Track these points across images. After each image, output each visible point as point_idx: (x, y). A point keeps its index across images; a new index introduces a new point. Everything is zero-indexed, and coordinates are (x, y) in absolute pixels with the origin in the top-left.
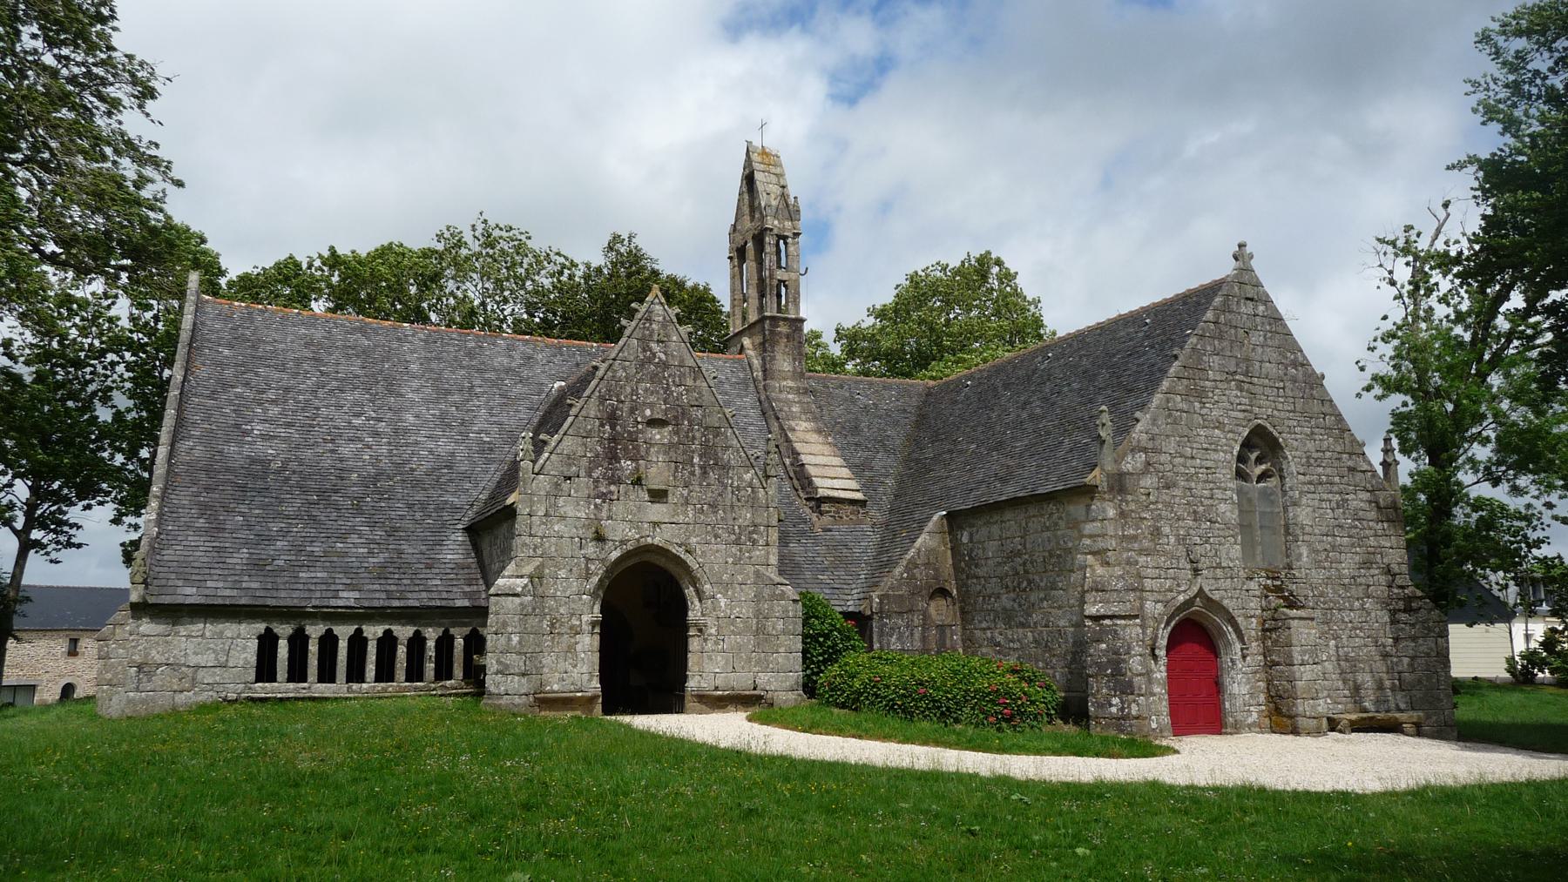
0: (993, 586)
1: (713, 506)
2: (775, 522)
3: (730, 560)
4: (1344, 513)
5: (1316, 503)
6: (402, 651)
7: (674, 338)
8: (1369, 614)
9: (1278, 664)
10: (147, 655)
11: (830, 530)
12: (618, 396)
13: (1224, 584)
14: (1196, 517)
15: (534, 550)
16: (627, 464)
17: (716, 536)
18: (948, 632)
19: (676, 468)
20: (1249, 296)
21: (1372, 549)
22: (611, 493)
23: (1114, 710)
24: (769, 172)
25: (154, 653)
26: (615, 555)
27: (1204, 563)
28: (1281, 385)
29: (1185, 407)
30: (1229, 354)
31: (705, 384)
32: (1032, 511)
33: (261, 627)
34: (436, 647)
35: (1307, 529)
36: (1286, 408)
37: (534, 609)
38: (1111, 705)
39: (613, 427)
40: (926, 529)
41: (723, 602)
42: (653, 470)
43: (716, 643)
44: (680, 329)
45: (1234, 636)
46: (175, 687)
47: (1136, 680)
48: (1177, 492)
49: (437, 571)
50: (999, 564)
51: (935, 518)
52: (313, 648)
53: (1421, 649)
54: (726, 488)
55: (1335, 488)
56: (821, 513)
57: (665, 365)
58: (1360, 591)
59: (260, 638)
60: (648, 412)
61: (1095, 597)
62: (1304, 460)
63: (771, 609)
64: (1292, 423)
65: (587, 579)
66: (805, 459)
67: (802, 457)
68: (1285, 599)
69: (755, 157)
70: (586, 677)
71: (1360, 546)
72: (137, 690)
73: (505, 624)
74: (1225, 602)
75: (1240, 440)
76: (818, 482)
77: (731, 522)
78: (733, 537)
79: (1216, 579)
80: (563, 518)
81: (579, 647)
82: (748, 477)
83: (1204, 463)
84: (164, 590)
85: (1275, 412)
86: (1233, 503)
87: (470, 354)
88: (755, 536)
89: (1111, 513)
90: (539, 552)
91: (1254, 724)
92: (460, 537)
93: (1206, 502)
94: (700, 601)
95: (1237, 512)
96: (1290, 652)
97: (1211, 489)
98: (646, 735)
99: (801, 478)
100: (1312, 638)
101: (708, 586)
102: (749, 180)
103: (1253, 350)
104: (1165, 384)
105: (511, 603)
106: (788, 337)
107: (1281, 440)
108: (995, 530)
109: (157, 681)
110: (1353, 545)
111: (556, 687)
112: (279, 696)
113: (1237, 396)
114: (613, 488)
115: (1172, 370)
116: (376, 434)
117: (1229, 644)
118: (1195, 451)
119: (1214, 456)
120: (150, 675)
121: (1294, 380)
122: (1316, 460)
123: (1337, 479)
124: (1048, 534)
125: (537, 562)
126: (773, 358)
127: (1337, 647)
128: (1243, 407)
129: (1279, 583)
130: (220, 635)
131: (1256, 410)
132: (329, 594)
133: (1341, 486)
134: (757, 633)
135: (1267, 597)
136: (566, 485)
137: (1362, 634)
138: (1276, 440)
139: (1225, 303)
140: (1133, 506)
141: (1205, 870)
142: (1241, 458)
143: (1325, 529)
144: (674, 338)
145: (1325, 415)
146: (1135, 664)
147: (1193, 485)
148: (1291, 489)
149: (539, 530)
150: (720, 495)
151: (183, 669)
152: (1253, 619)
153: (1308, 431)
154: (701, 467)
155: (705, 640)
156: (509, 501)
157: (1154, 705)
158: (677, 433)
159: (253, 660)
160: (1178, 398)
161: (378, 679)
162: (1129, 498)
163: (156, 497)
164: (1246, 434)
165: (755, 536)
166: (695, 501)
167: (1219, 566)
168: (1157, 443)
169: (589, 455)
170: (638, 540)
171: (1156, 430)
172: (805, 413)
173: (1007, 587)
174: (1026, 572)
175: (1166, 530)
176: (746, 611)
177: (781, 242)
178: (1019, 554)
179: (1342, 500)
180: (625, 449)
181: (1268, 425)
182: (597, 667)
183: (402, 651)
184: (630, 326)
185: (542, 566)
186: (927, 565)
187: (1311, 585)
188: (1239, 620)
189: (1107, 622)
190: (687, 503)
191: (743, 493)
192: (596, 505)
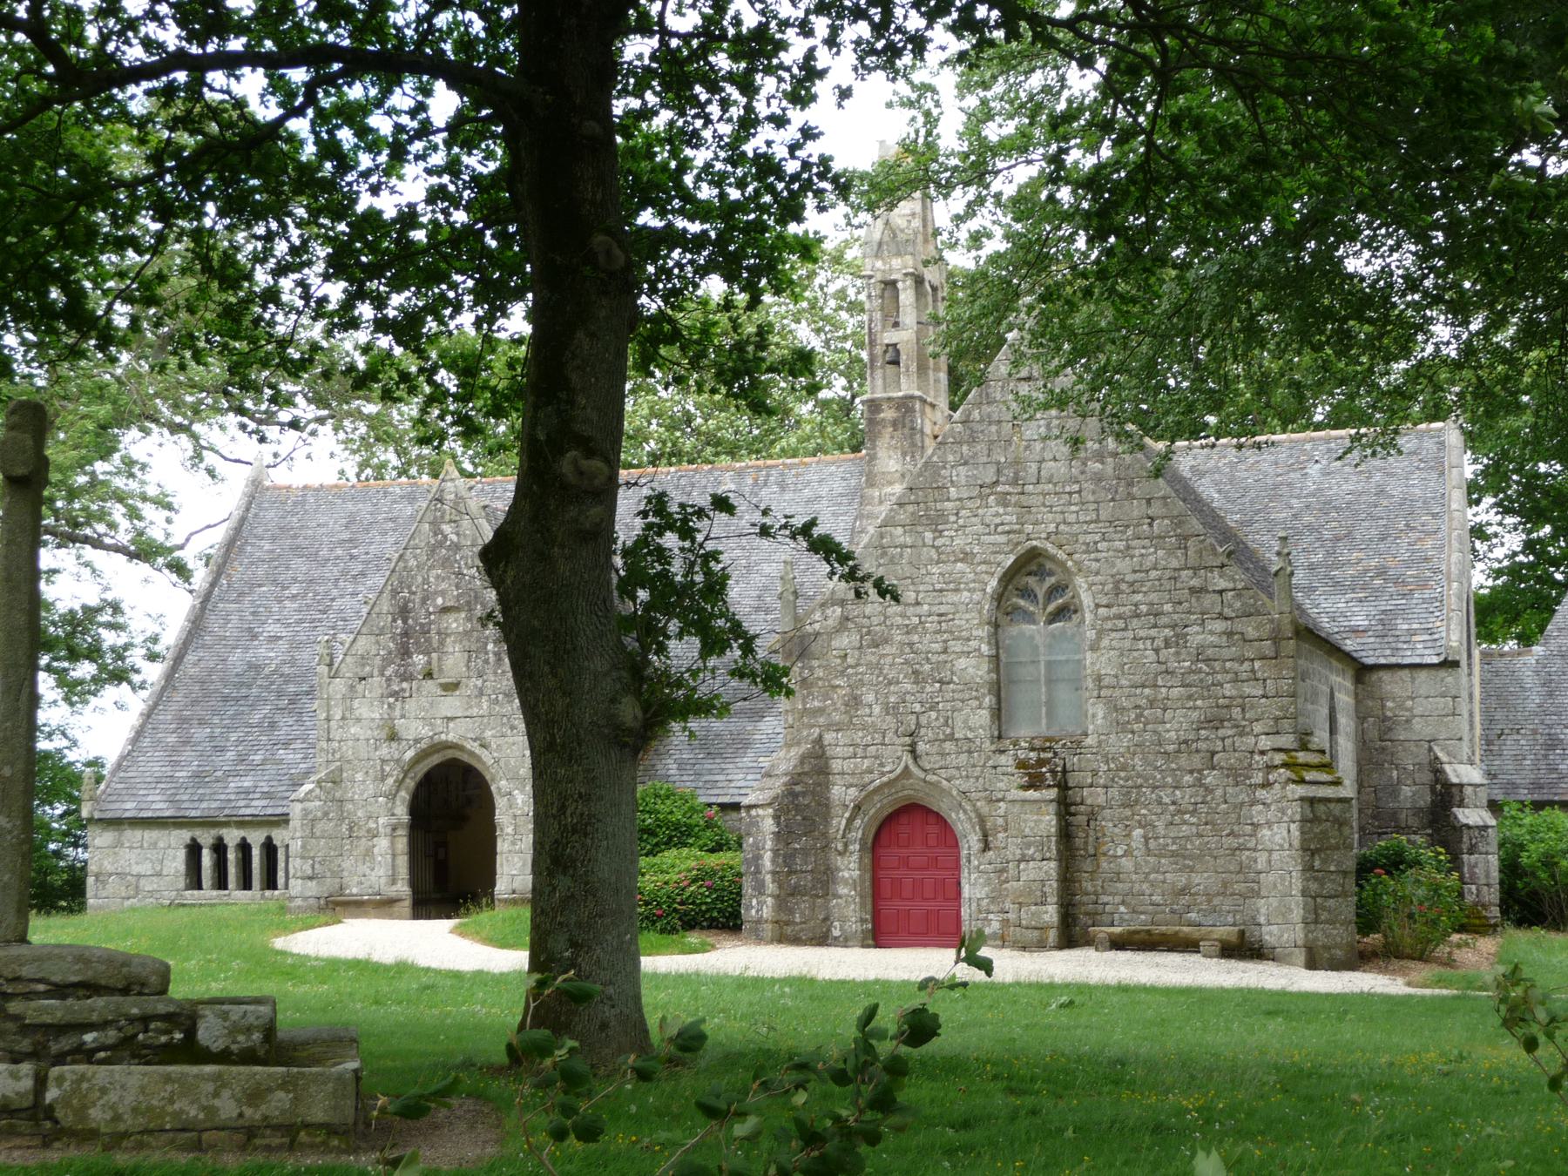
4: (1177, 653)
12: (409, 587)
16: (419, 659)
21: (1226, 701)
22: (403, 690)
28: (1076, 487)
29: (909, 541)
33: (185, 835)
39: (405, 622)
43: (513, 843)
48: (887, 649)
55: (1164, 620)
57: (457, 547)
58: (1197, 762)
59: (188, 846)
64: (1089, 538)
70: (383, 881)
75: (1000, 571)
81: (376, 850)
83: (935, 609)
85: (1062, 527)
86: (982, 655)
90: (337, 756)
93: (934, 658)
97: (945, 641)
100: (1042, 826)
103: (1027, 448)
107: (1070, 563)
109: (110, 889)
110: (1190, 697)
111: (355, 891)
113: (997, 515)
114: (405, 685)
119: (955, 598)
120: (104, 883)
122: (1132, 584)
123: (1168, 607)
127: (1146, 839)
128: (1007, 528)
129: (1050, 755)
130: (154, 845)
133: (1175, 617)
136: (360, 688)
137: (1194, 820)
140: (820, 673)
143: (1137, 679)
145: (1152, 519)
147: (916, 638)
153: (1121, 545)
160: (900, 530)
162: (815, 663)
164: (1009, 562)
175: (870, 698)
179: (1177, 635)
180: (417, 643)
187: (1106, 756)
190: (481, 694)
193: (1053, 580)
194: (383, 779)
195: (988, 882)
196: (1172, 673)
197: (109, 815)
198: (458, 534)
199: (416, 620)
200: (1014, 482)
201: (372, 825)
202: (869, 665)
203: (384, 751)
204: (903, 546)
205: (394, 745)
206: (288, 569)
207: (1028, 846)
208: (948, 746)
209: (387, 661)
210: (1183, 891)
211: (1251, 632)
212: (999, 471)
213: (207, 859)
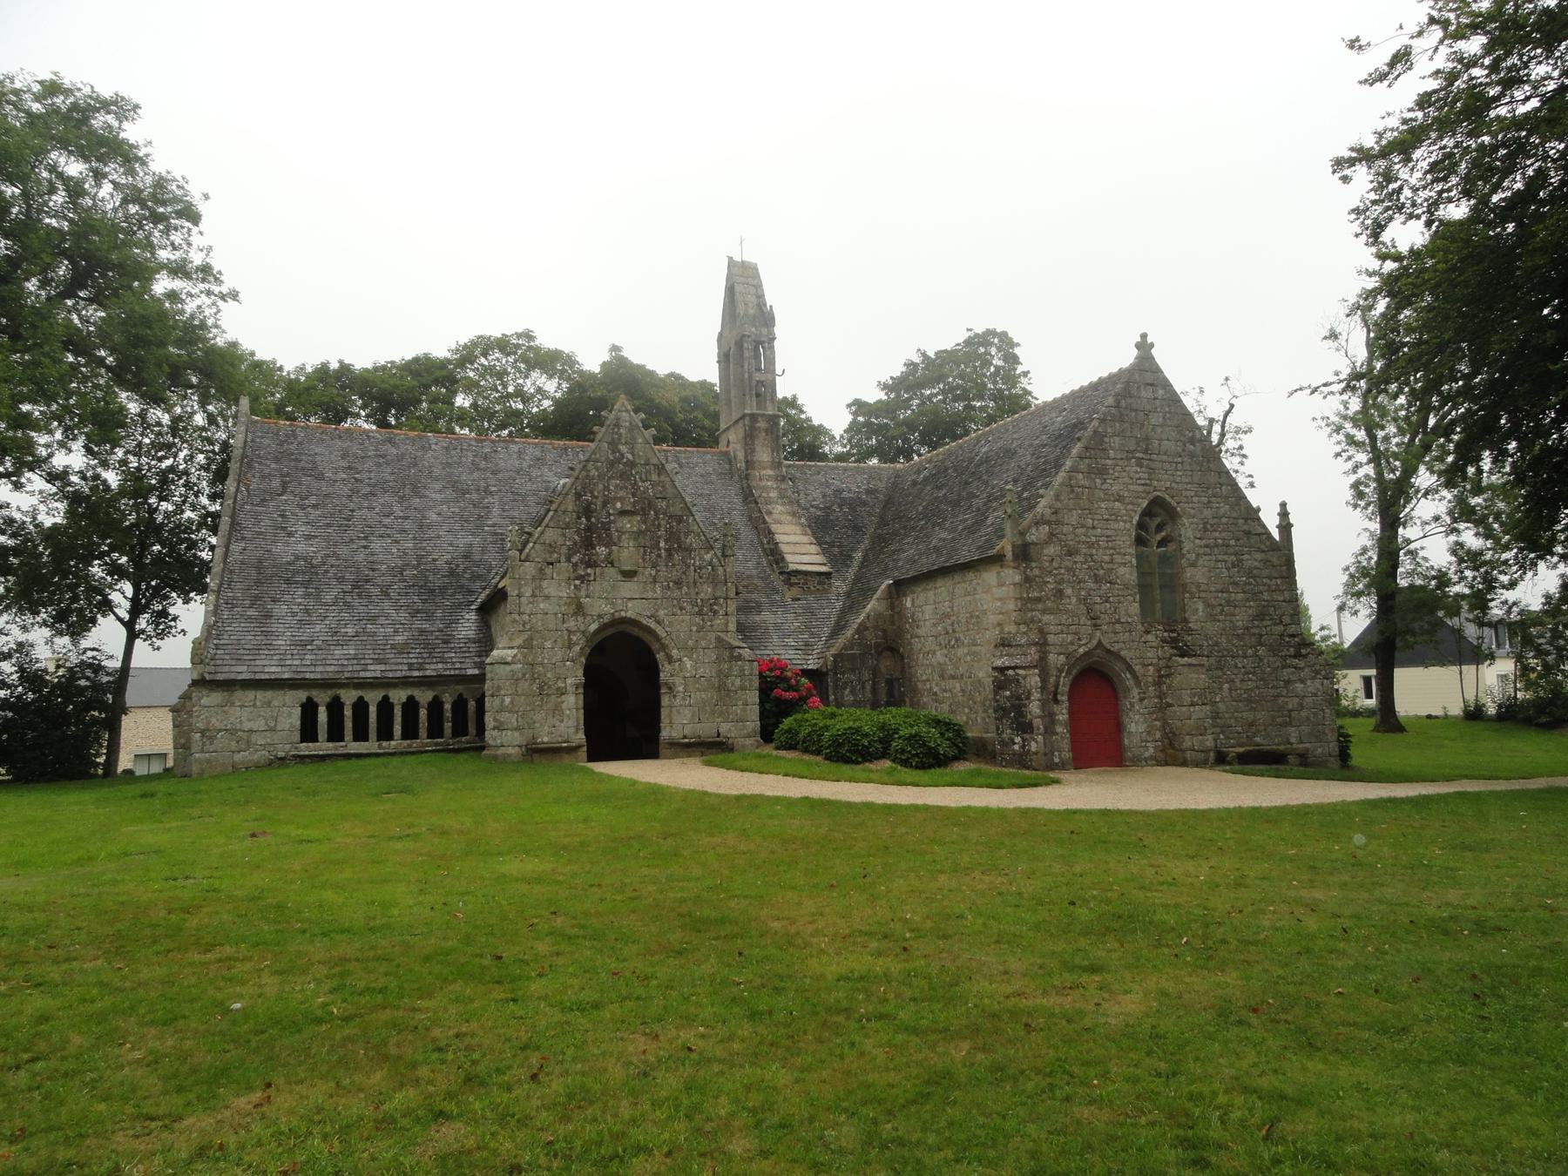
0: (930, 644)
1: (678, 583)
2: (732, 594)
3: (694, 629)
6: (423, 713)
8: (1261, 660)
9: (1171, 705)
10: (209, 722)
11: (799, 599)
12: (592, 492)
13: (1122, 637)
16: (601, 550)
17: (681, 609)
19: (645, 552)
20: (1150, 381)
22: (589, 575)
23: (1016, 747)
25: (214, 721)
26: (594, 627)
28: (1179, 460)
29: (1087, 483)
30: (1129, 434)
32: (957, 578)
33: (302, 695)
35: (1203, 587)
36: (1184, 480)
37: (524, 675)
39: (588, 519)
40: (875, 596)
41: (688, 664)
42: (625, 554)
43: (684, 699)
44: (645, 432)
45: (1132, 682)
46: (233, 749)
48: (1079, 558)
50: (934, 625)
51: (883, 587)
52: (348, 712)
56: (791, 585)
57: (632, 464)
59: (303, 706)
60: (619, 505)
63: (730, 669)
64: (1188, 493)
65: (570, 648)
66: (779, 538)
70: (572, 730)
71: (1253, 600)
72: (202, 751)
73: (499, 688)
74: (1123, 653)
75: (1139, 510)
76: (789, 558)
77: (694, 596)
78: (696, 609)
79: (1116, 633)
81: (564, 706)
82: (708, 557)
84: (219, 669)
86: (1132, 566)
87: (486, 458)
90: (528, 627)
91: (1151, 758)
92: (473, 616)
93: (1105, 566)
96: (1042, 693)
99: (774, 554)
102: (730, 292)
105: (503, 670)
106: (766, 431)
108: (931, 594)
109: (218, 744)
110: (1247, 600)
111: (546, 739)
113: (1137, 472)
114: (589, 571)
117: (1127, 690)
120: (212, 738)
122: (1212, 525)
123: (1232, 542)
124: (968, 598)
125: (526, 635)
127: (1230, 690)
130: (268, 704)
132: (358, 668)
134: (719, 689)
136: (549, 570)
138: (1175, 509)
140: (1037, 572)
142: (1141, 526)
143: (1219, 587)
146: (1034, 708)
148: (1189, 552)
150: (684, 573)
153: (1205, 500)
154: (666, 550)
155: (675, 696)
158: (645, 522)
159: (298, 723)
160: (1081, 476)
161: (405, 736)
162: (1034, 565)
164: (1145, 505)
167: (1118, 622)
168: (1060, 516)
171: (1059, 505)
174: (954, 631)
175: (1069, 591)
176: (707, 671)
180: (599, 537)
182: (582, 722)
183: (423, 713)
184: (712, 409)
185: (531, 639)
186: (876, 627)
188: (1137, 668)
189: (1011, 672)
190: (655, 581)
192: (575, 586)
193: (1159, 519)
194: (570, 646)
195: (1145, 721)
197: (220, 677)
198: (632, 454)
199: (598, 519)
200: (1146, 452)
201: (561, 684)
202: (1069, 570)
203: (571, 624)
205: (580, 619)
206: (300, 484)
207: (1194, 695)
208: (1117, 626)
209: (572, 552)
210: (1251, 724)
211: (1276, 561)
212: (1138, 443)
213: (323, 716)
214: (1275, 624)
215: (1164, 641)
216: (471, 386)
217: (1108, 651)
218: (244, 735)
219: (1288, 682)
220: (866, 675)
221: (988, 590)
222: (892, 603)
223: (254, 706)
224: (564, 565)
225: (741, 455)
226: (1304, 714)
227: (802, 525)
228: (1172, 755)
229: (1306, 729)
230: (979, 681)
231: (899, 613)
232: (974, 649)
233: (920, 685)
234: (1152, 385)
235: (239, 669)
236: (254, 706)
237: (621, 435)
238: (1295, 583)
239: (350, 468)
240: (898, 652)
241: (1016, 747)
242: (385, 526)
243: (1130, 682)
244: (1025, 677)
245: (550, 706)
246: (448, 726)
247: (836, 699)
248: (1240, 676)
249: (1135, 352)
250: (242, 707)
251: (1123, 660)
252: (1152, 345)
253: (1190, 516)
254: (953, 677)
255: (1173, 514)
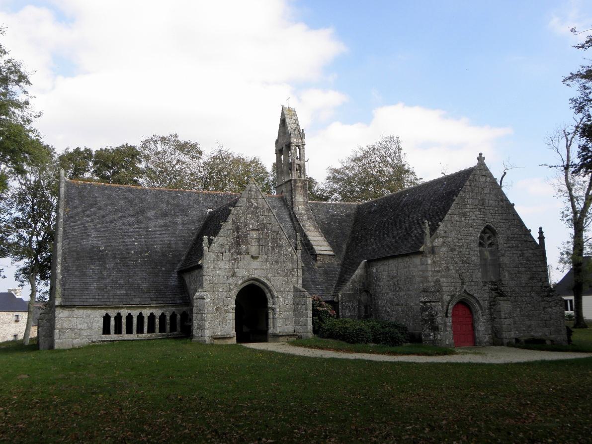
1: (277, 262)
3: (284, 283)
4: (523, 258)
5: (511, 255)
6: (157, 321)
7: (260, 197)
8: (533, 298)
10: (62, 325)
12: (239, 221)
14: (463, 262)
15: (210, 281)
16: (244, 247)
17: (278, 273)
18: (369, 308)
20: (484, 174)
21: (534, 272)
22: (238, 258)
23: (431, 337)
24: (291, 118)
25: (65, 324)
26: (240, 282)
27: (466, 280)
29: (458, 219)
31: (272, 215)
32: (400, 260)
33: (104, 312)
34: (170, 319)
35: (508, 265)
38: (430, 336)
39: (238, 233)
40: (359, 267)
45: (479, 308)
46: (73, 337)
47: (440, 326)
49: (169, 289)
52: (124, 321)
53: (554, 311)
54: (281, 255)
55: (519, 249)
57: (257, 208)
58: (530, 289)
59: (104, 317)
60: (251, 226)
61: (424, 295)
62: (506, 238)
65: (230, 292)
67: (309, 237)
68: (498, 293)
69: (285, 112)
72: (59, 338)
74: (475, 295)
75: (480, 231)
78: (285, 274)
80: (220, 268)
82: (289, 250)
88: (293, 273)
89: (430, 262)
94: (273, 298)
95: (479, 259)
98: (254, 350)
101: (275, 293)
102: (283, 121)
104: (450, 211)
108: (386, 267)
111: (219, 334)
112: (112, 339)
114: (238, 256)
115: (453, 205)
116: (139, 234)
118: (462, 237)
120: (64, 333)
121: (502, 207)
123: (520, 245)
124: (406, 269)
126: (295, 197)
127: (520, 311)
131: (487, 219)
135: (491, 292)
139: (474, 178)
140: (438, 259)
141: (558, 420)
142: (481, 237)
144: (260, 197)
146: (439, 320)
149: (212, 274)
150: (279, 257)
151: (76, 330)
152: (486, 301)
154: (271, 247)
156: (200, 263)
157: (446, 336)
159: (102, 326)
160: (455, 216)
161: (148, 332)
162: (437, 256)
163: (59, 263)
165: (293, 273)
166: (270, 260)
169: (229, 244)
170: (248, 276)
171: (446, 229)
172: (309, 219)
173: (391, 290)
177: (297, 148)
178: (395, 277)
181: (491, 225)
182: (234, 325)
183: (157, 321)
186: (360, 282)
188: (481, 302)
189: (428, 304)
191: (288, 256)
192: (232, 263)
196: (522, 264)
198: (257, 203)
202: (451, 258)
204: (457, 221)
205: (234, 278)
208: (472, 283)
211: (538, 254)
212: (479, 201)
214: (538, 282)
215: (492, 289)
216: (147, 158)
217: (468, 294)
218: (78, 331)
219: (544, 308)
220: (356, 304)
221: (416, 266)
222: (366, 270)
223: (83, 317)
224: (227, 254)
225: (289, 198)
226: (552, 322)
227: (319, 231)
228: (497, 341)
229: (552, 329)
230: (411, 307)
231: (370, 274)
232: (408, 292)
233: (380, 308)
234: (485, 176)
235: (77, 300)
236: (83, 317)
237: (252, 195)
238: (546, 263)
239: (112, 204)
240: (369, 292)
241: (431, 337)
242: (131, 232)
243: (478, 308)
244: (435, 306)
245: (221, 318)
246: (168, 327)
247: (342, 314)
248: (524, 305)
249: (477, 161)
250: (77, 318)
251: (474, 298)
252: (484, 158)
253: (502, 234)
254: (398, 305)
255: (494, 233)
